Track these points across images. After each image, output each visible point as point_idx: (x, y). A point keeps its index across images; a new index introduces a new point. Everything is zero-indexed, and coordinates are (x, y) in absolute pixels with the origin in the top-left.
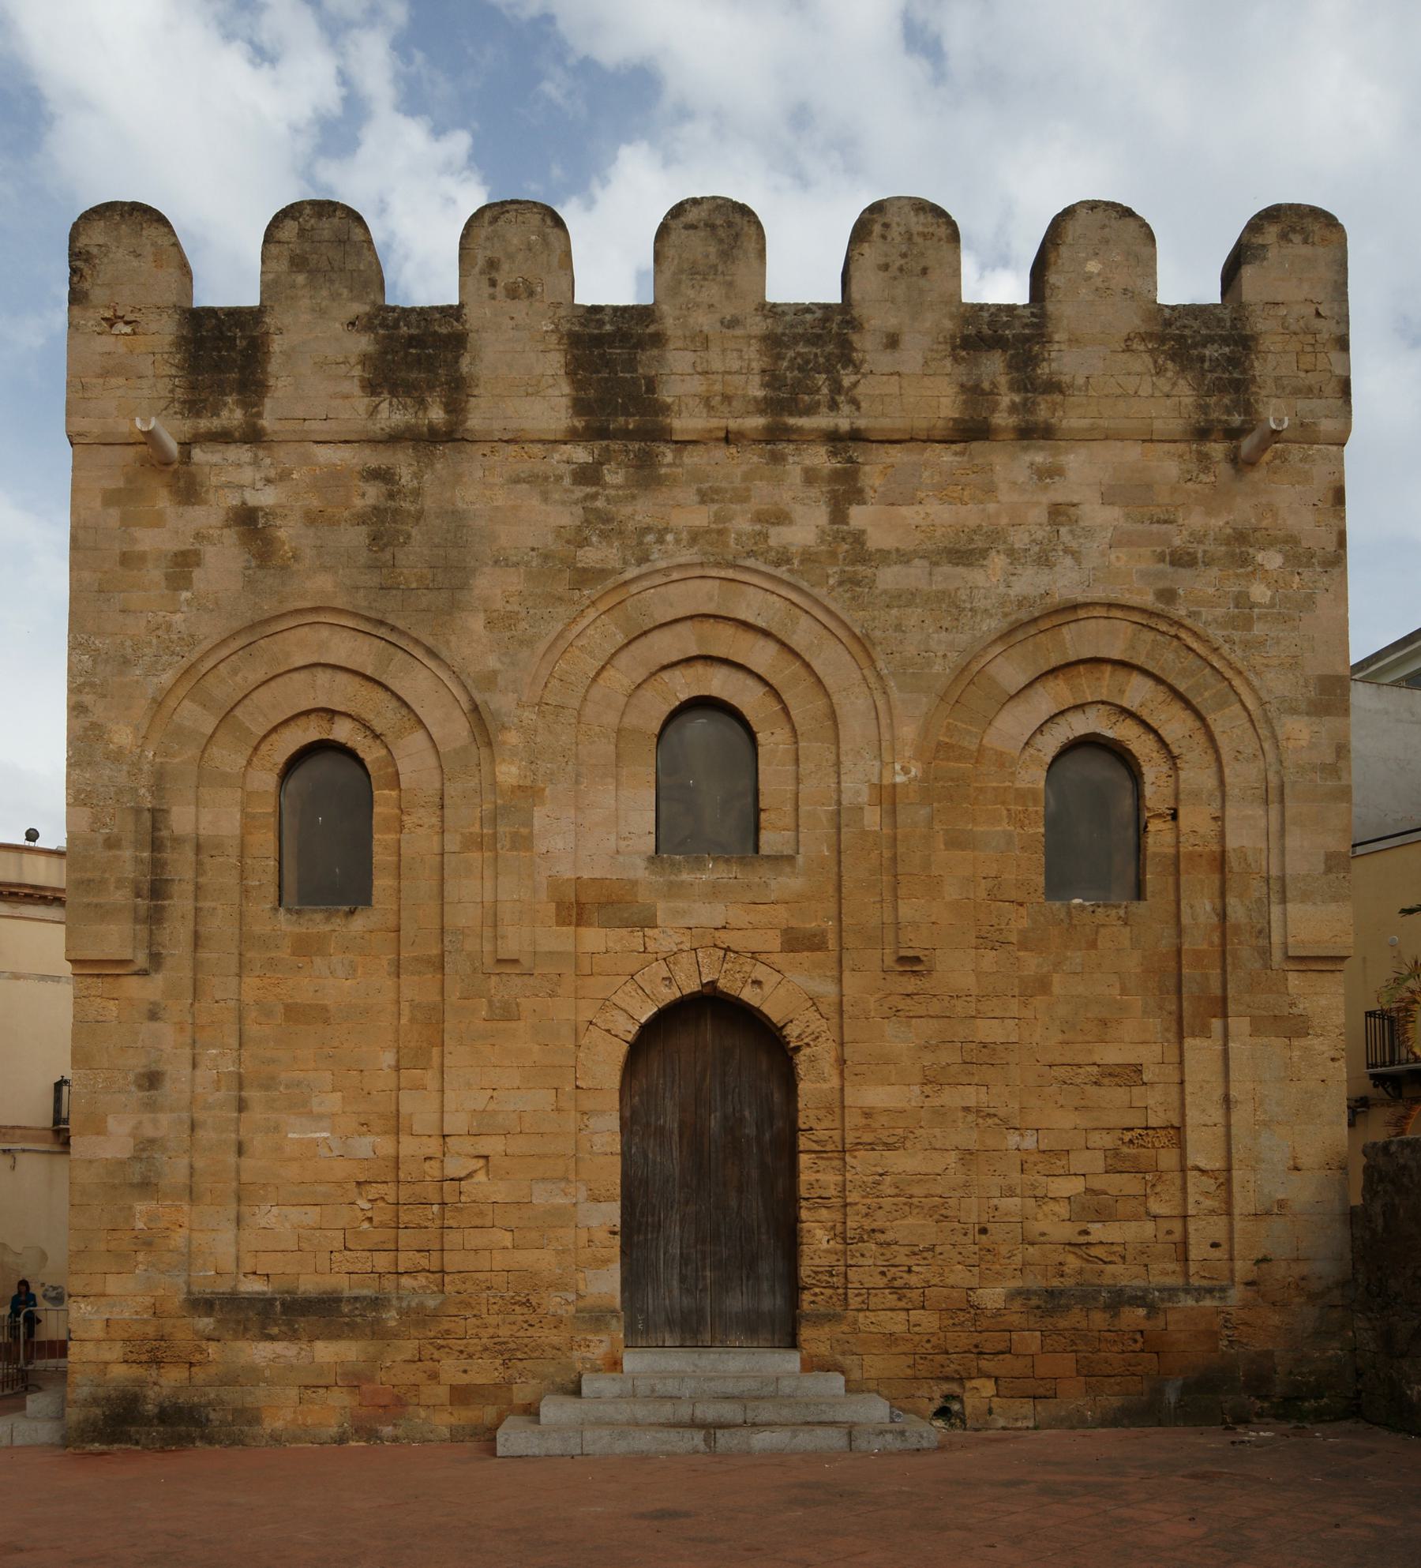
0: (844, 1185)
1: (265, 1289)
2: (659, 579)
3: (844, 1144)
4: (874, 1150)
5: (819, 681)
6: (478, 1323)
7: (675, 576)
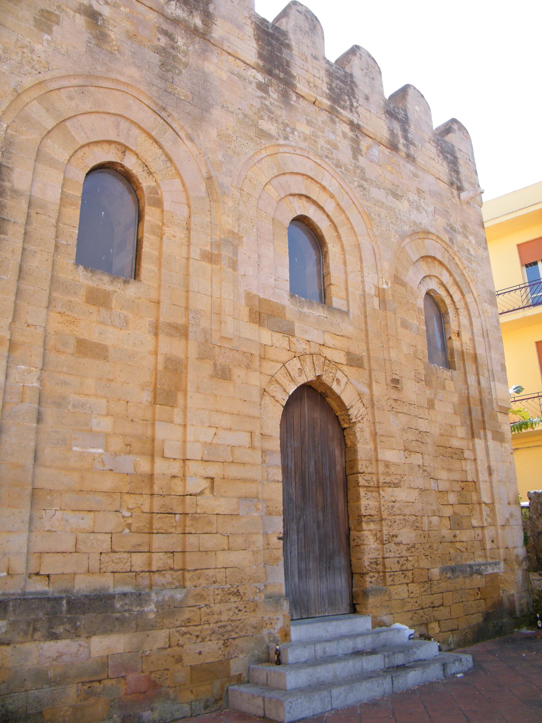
0: (380, 508)
1: (46, 588)
2: (290, 150)
3: (378, 482)
4: (390, 487)
5: (352, 228)
6: (208, 611)
7: (298, 152)
